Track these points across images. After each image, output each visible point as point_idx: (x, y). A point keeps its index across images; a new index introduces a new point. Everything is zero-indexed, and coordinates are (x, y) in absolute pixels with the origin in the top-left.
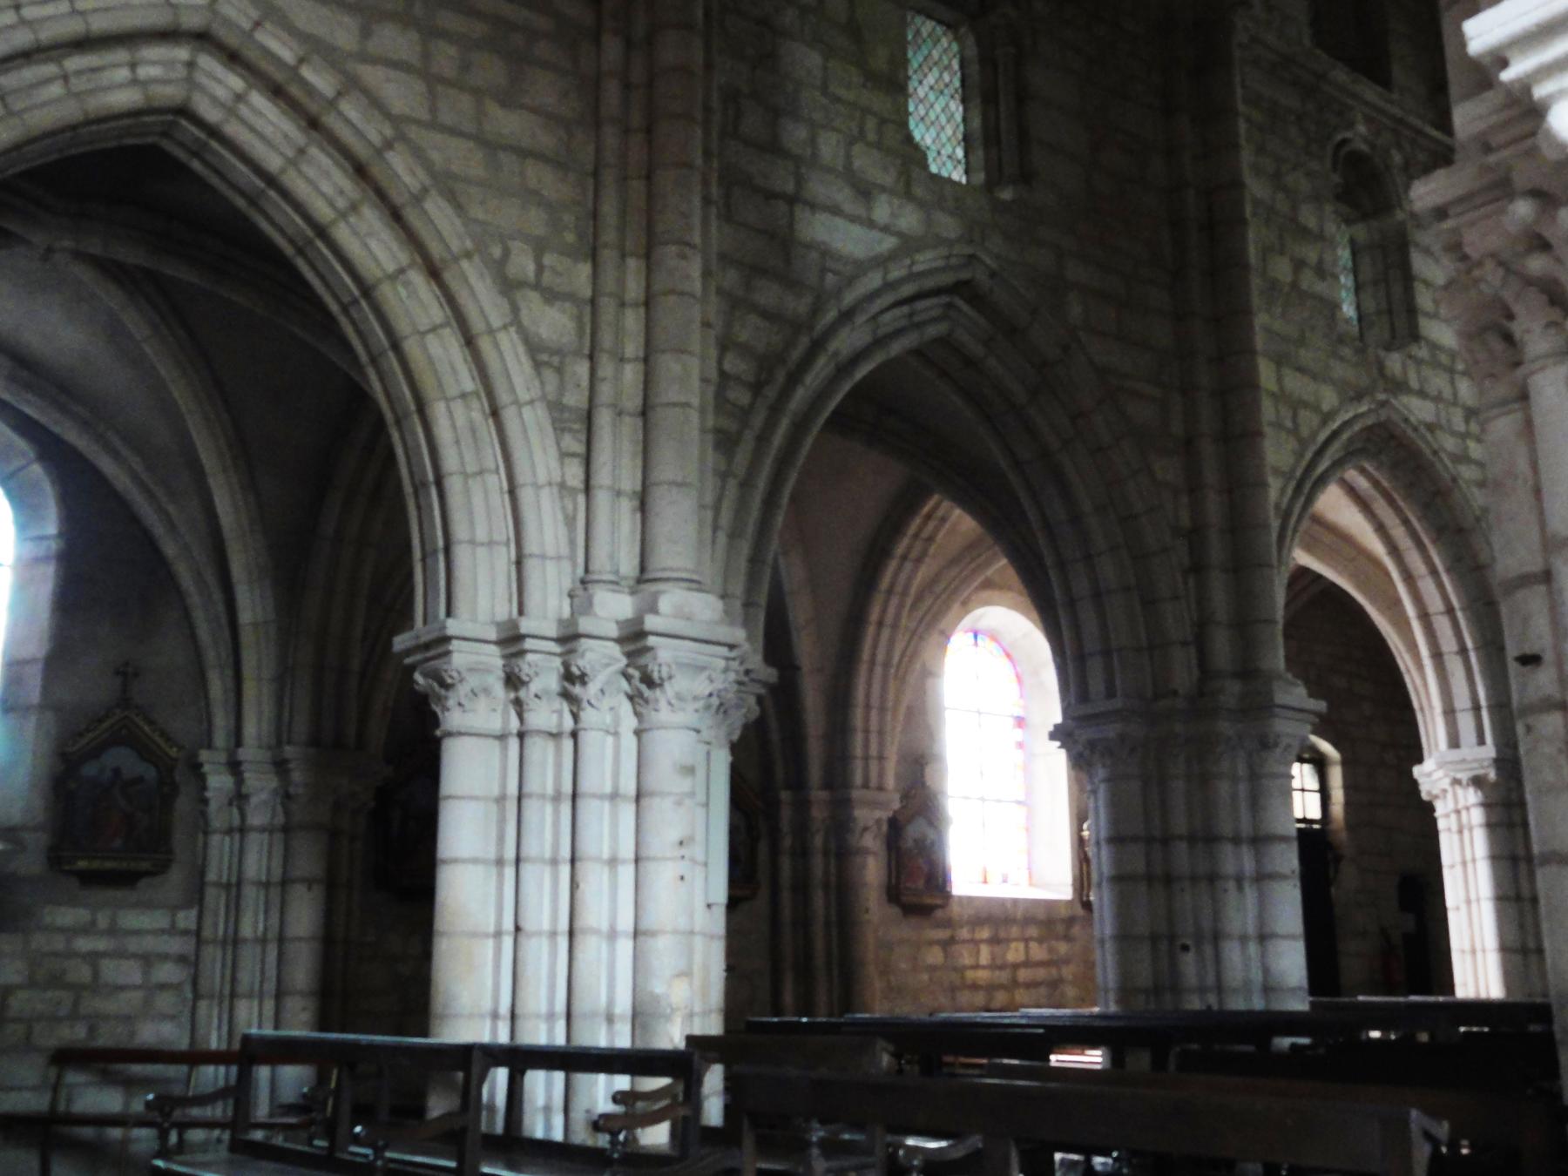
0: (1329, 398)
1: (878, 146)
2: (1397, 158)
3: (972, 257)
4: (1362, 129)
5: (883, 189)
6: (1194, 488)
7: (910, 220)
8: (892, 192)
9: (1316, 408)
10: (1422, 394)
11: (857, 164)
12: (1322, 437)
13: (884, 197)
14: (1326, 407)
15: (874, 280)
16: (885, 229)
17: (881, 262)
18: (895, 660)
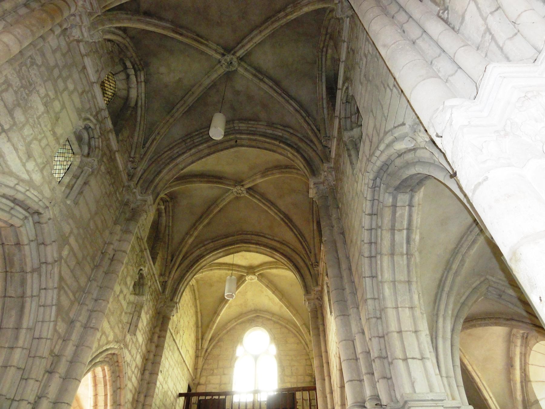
0: (111, 338)
1: (43, 149)
2: (149, 284)
3: (47, 207)
4: (146, 269)
5: (35, 160)
6: (65, 340)
7: (37, 178)
8: (37, 164)
9: (107, 337)
10: (130, 352)
11: (32, 146)
12: (104, 348)
13: (34, 163)
14: (109, 339)
15: (12, 182)
16: (27, 171)
17: (21, 181)
18: (291, 101)
